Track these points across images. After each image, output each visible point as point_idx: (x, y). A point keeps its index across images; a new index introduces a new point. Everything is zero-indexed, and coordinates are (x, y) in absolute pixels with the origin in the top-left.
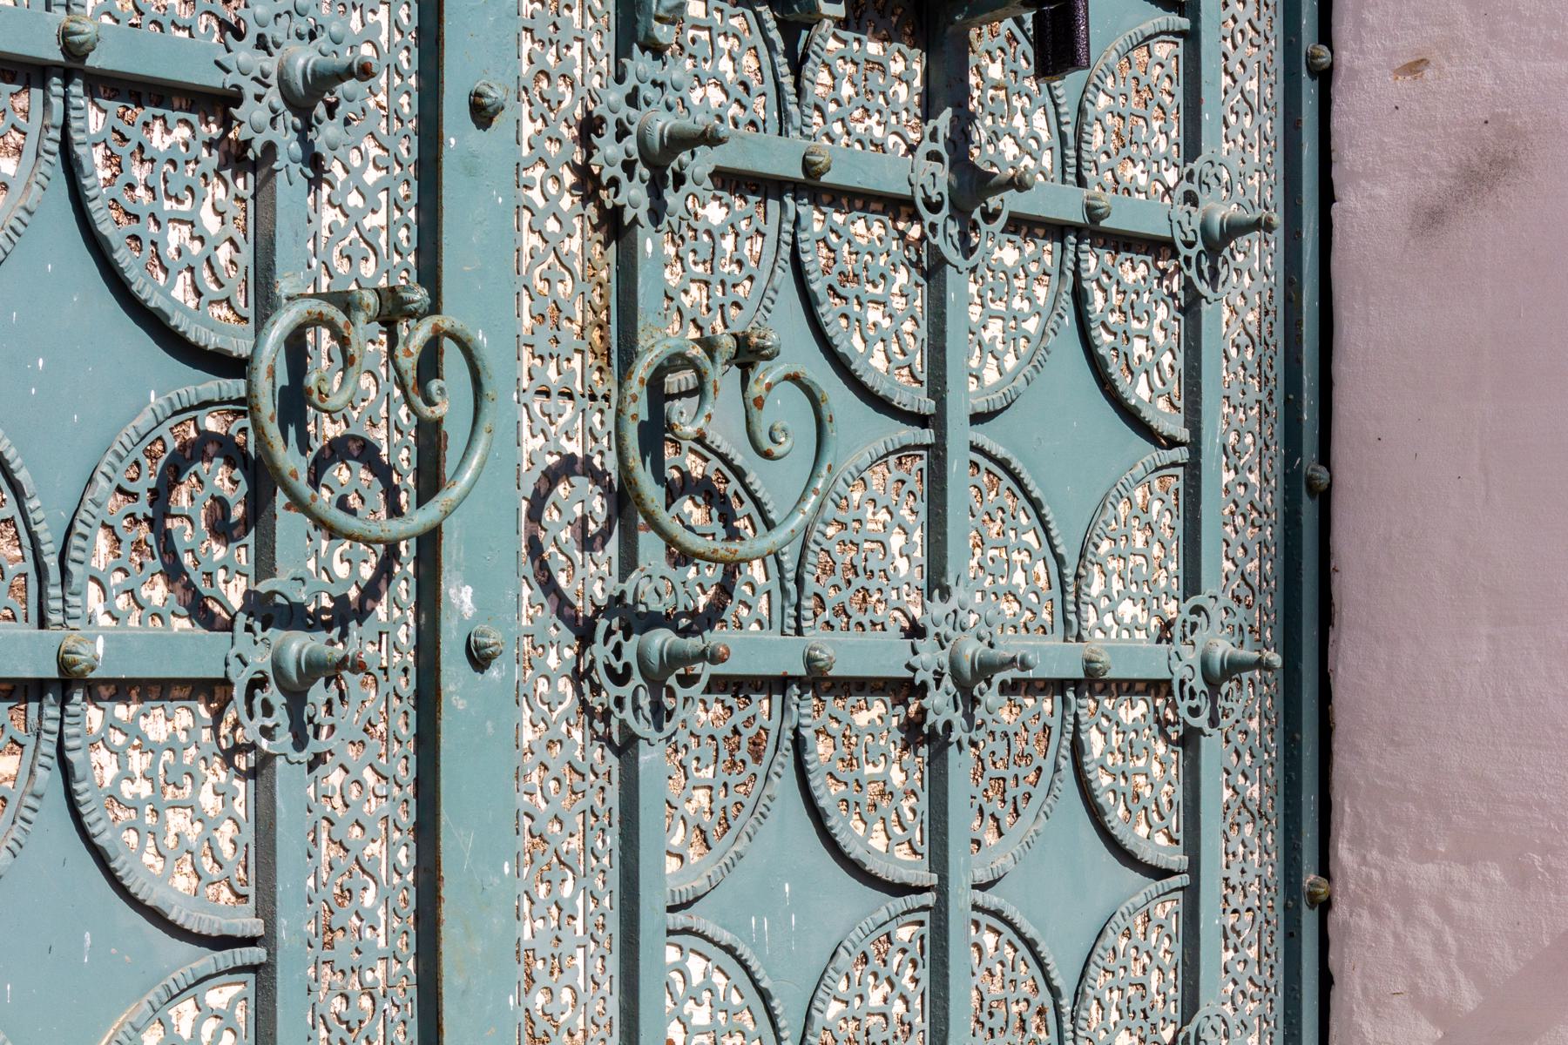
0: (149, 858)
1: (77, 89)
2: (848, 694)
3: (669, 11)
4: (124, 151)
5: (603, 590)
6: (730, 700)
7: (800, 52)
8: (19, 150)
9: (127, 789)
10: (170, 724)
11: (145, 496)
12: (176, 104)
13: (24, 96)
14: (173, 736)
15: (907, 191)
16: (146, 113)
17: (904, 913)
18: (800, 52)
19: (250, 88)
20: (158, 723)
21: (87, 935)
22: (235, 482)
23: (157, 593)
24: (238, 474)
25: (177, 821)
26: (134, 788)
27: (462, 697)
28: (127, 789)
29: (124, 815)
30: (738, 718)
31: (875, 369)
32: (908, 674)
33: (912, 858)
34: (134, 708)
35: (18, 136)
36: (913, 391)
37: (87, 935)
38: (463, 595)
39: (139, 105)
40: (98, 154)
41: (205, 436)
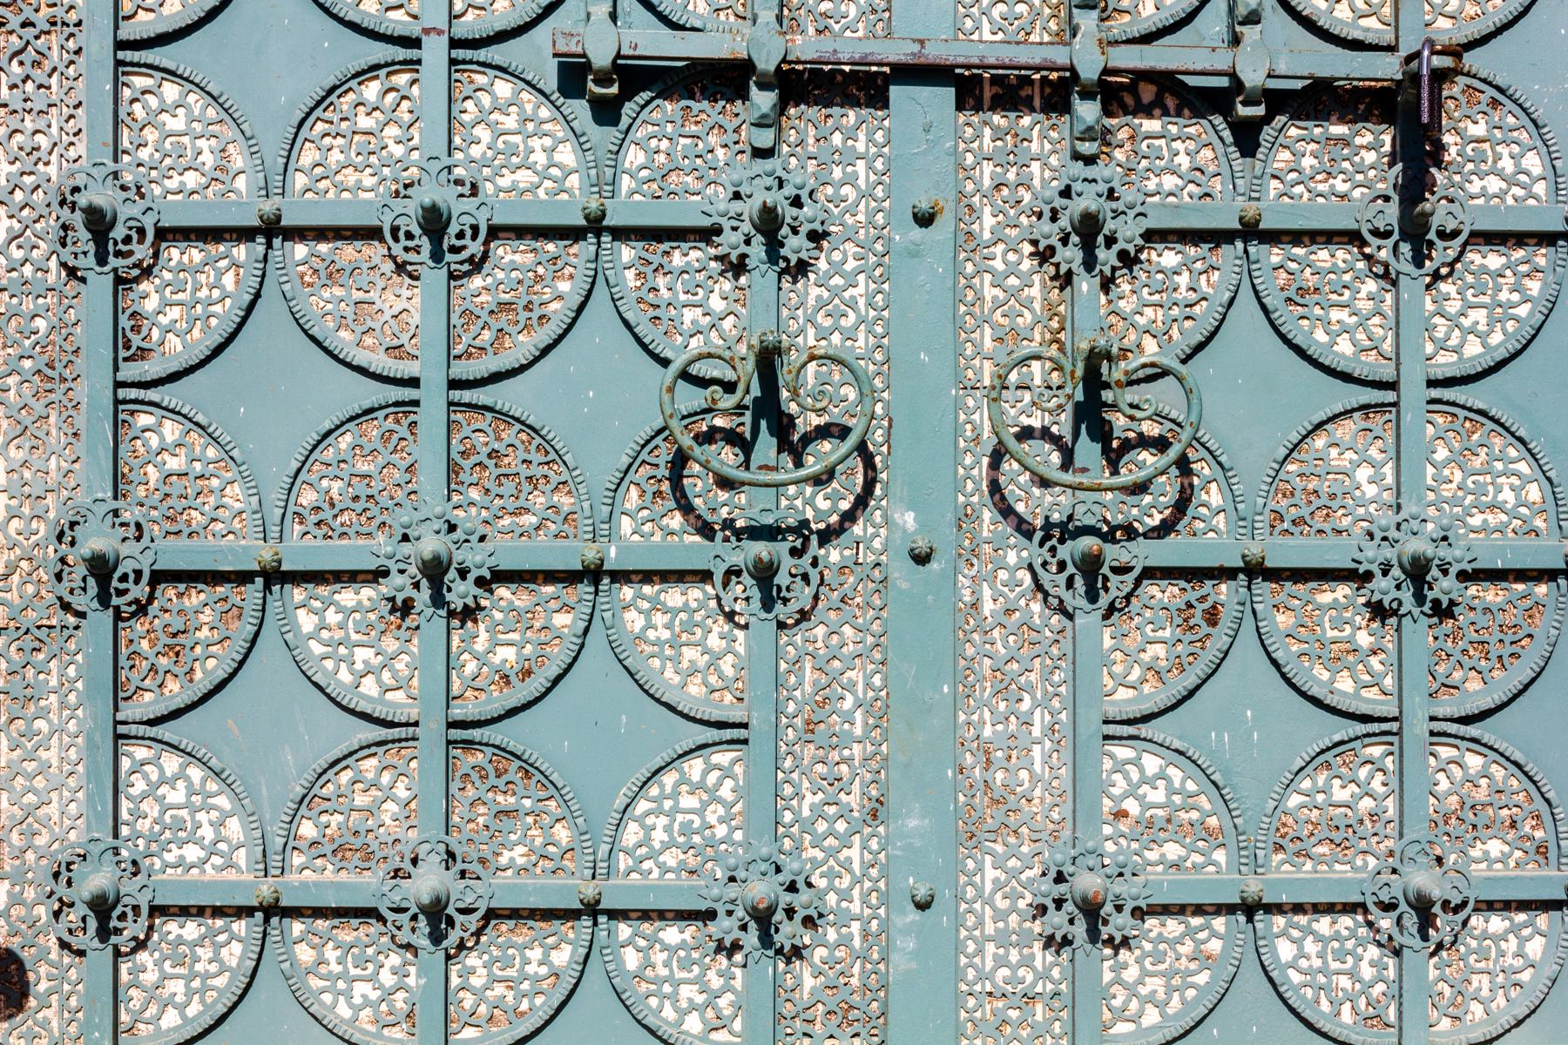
0: (669, 673)
1: (606, 238)
2: (1306, 581)
3: (1082, 133)
4: (649, 270)
5: (56, 551)
6: (1183, 584)
7: (685, 63)
8: (571, 277)
9: (651, 634)
10: (684, 597)
11: (662, 465)
12: (692, 238)
13: (575, 246)
14: (686, 604)
15: (1355, 226)
16: (666, 246)
17: (1318, 754)
18: (685, 63)
19: (727, 225)
20: (674, 596)
21: (624, 717)
22: (737, 455)
23: (676, 521)
24: (737, 450)
25: (689, 654)
26: (657, 634)
27: (905, 581)
28: (651, 634)
29: (648, 649)
30: (1192, 596)
31: (1343, 356)
32: (1354, 565)
33: (1383, 697)
34: (657, 588)
35: (571, 269)
36: (1384, 366)
37: (624, 717)
38: (906, 517)
39: (660, 242)
40: (630, 274)
41: (713, 430)
